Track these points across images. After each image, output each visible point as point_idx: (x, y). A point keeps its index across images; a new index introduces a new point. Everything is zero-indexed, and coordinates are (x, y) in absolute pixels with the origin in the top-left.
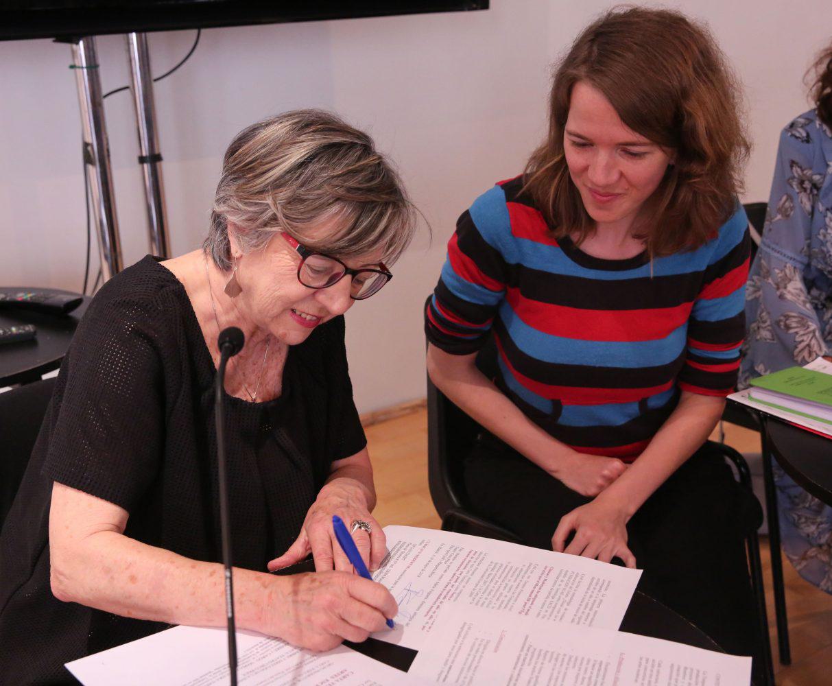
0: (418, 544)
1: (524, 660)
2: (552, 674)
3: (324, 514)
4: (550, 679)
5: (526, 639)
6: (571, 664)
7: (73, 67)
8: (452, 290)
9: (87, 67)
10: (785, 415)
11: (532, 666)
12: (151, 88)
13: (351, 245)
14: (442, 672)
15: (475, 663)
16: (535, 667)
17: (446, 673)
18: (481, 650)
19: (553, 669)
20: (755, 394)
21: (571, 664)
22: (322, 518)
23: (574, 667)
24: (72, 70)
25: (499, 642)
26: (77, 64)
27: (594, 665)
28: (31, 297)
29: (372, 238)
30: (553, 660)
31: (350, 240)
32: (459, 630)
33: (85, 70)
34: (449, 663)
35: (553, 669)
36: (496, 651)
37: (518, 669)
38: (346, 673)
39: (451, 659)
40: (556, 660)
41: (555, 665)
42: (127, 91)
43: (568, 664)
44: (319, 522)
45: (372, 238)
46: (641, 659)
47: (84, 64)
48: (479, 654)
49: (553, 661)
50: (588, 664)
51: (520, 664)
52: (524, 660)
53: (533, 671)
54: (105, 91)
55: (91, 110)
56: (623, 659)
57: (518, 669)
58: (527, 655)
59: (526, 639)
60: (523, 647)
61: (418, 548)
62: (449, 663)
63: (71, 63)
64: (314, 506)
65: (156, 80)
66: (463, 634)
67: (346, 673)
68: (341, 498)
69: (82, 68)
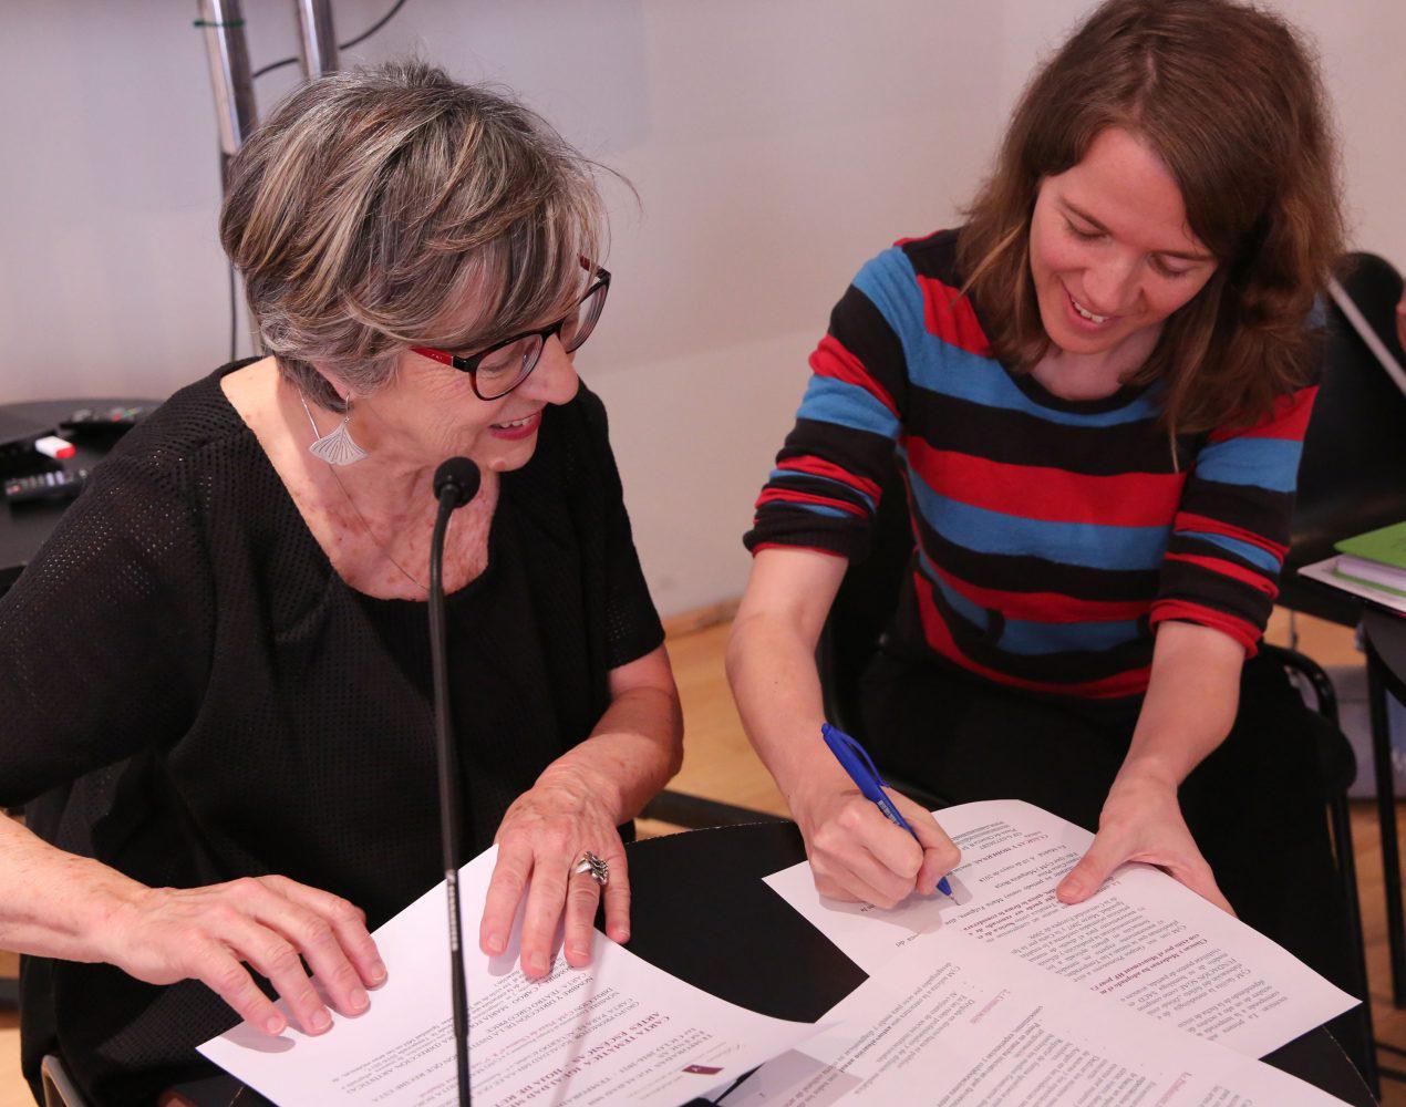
0: (1024, 834)
1: (1013, 1046)
2: (1049, 1078)
3: (538, 817)
4: (1041, 1086)
5: (1037, 1011)
6: (1090, 1070)
7: (200, 24)
8: (837, 467)
9: (225, 25)
10: (1390, 599)
11: (1021, 1059)
12: (1349, 622)
13: (522, 309)
14: (871, 1033)
15: (931, 1032)
16: (1025, 1061)
17: (876, 1036)
18: (950, 1014)
19: (1053, 1072)
20: (1345, 567)
21: (1090, 1070)
22: (531, 822)
23: (1091, 1077)
24: (199, 31)
25: (988, 1008)
26: (207, 18)
27: (1126, 1082)
28: (135, 416)
29: (547, 278)
30: (1063, 1057)
31: (519, 299)
32: (935, 972)
33: (221, 31)
34: (889, 1023)
35: (1053, 1072)
36: (974, 1021)
37: (994, 1058)
38: (657, 1019)
39: (895, 1016)
40: (1068, 1057)
41: (1061, 1066)
42: (294, 68)
43: (1083, 1070)
44: (522, 827)
45: (547, 278)
46: (1216, 1089)
47: (219, 18)
48: (946, 1019)
49: (1061, 1059)
50: (1117, 1077)
51: (1003, 1050)
52: (1013, 1046)
53: (1019, 1067)
54: (255, 66)
55: (232, 98)
56: (1183, 1082)
57: (994, 1058)
58: (1023, 1037)
59: (1037, 1011)
60: (1023, 1025)
61: (1021, 839)
62: (889, 1023)
63: (195, 16)
64: (525, 796)
65: (344, 47)
66: (934, 983)
67: (657, 1019)
68: (573, 794)
69: (215, 25)
